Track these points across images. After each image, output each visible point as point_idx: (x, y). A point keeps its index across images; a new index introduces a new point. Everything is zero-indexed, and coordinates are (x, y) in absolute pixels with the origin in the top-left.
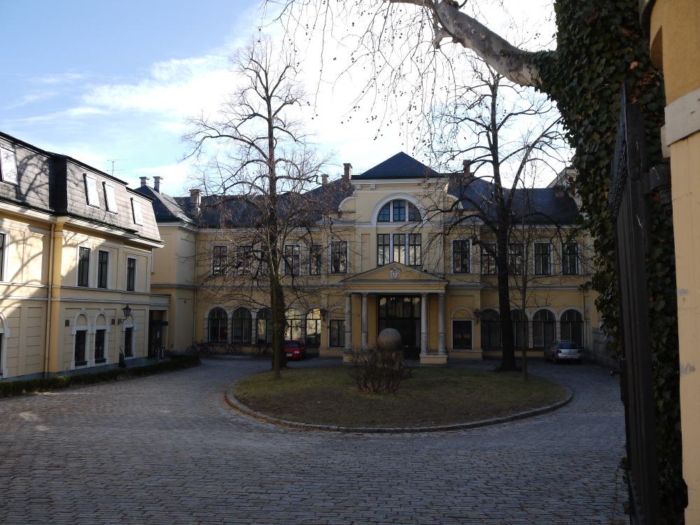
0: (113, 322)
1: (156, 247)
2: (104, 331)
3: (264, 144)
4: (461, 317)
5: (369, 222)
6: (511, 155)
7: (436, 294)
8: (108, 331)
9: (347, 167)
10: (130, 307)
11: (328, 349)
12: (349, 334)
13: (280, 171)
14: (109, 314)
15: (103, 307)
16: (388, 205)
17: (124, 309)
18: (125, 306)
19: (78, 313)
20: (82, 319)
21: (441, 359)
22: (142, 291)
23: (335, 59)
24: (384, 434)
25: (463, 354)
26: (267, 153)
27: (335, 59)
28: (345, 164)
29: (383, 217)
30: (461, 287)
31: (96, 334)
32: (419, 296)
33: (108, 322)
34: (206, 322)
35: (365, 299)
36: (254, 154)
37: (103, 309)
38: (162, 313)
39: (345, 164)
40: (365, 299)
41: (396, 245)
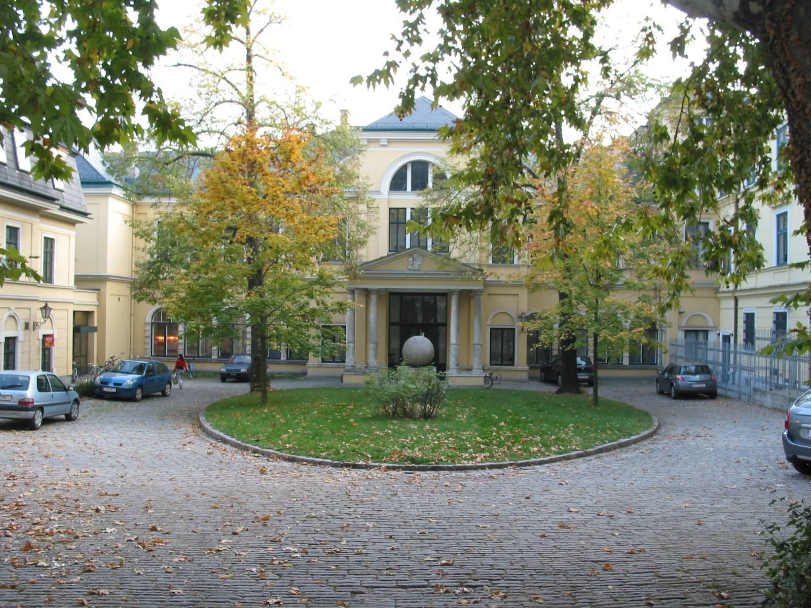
0: (27, 326)
1: (82, 222)
2: (14, 338)
3: (239, 78)
4: (503, 322)
5: (378, 192)
6: (190, 66)
7: (470, 291)
8: (21, 339)
9: (345, 113)
10: (50, 305)
11: (320, 367)
12: (352, 345)
13: (261, 113)
14: (22, 316)
15: (13, 305)
16: (405, 167)
17: (41, 309)
18: (43, 305)
19: (7, 313)
20: (12, 321)
21: (476, 379)
22: (65, 284)
23: (652, 5)
24: (442, 472)
25: (503, 372)
26: (245, 92)
27: (652, 5)
28: (342, 111)
29: (397, 184)
30: (499, 284)
31: (5, 343)
32: (445, 295)
33: (21, 326)
34: (149, 328)
35: (374, 298)
36: (227, 92)
37: (13, 308)
38: (88, 314)
39: (342, 111)
40: (374, 298)
41: (394, 223)
